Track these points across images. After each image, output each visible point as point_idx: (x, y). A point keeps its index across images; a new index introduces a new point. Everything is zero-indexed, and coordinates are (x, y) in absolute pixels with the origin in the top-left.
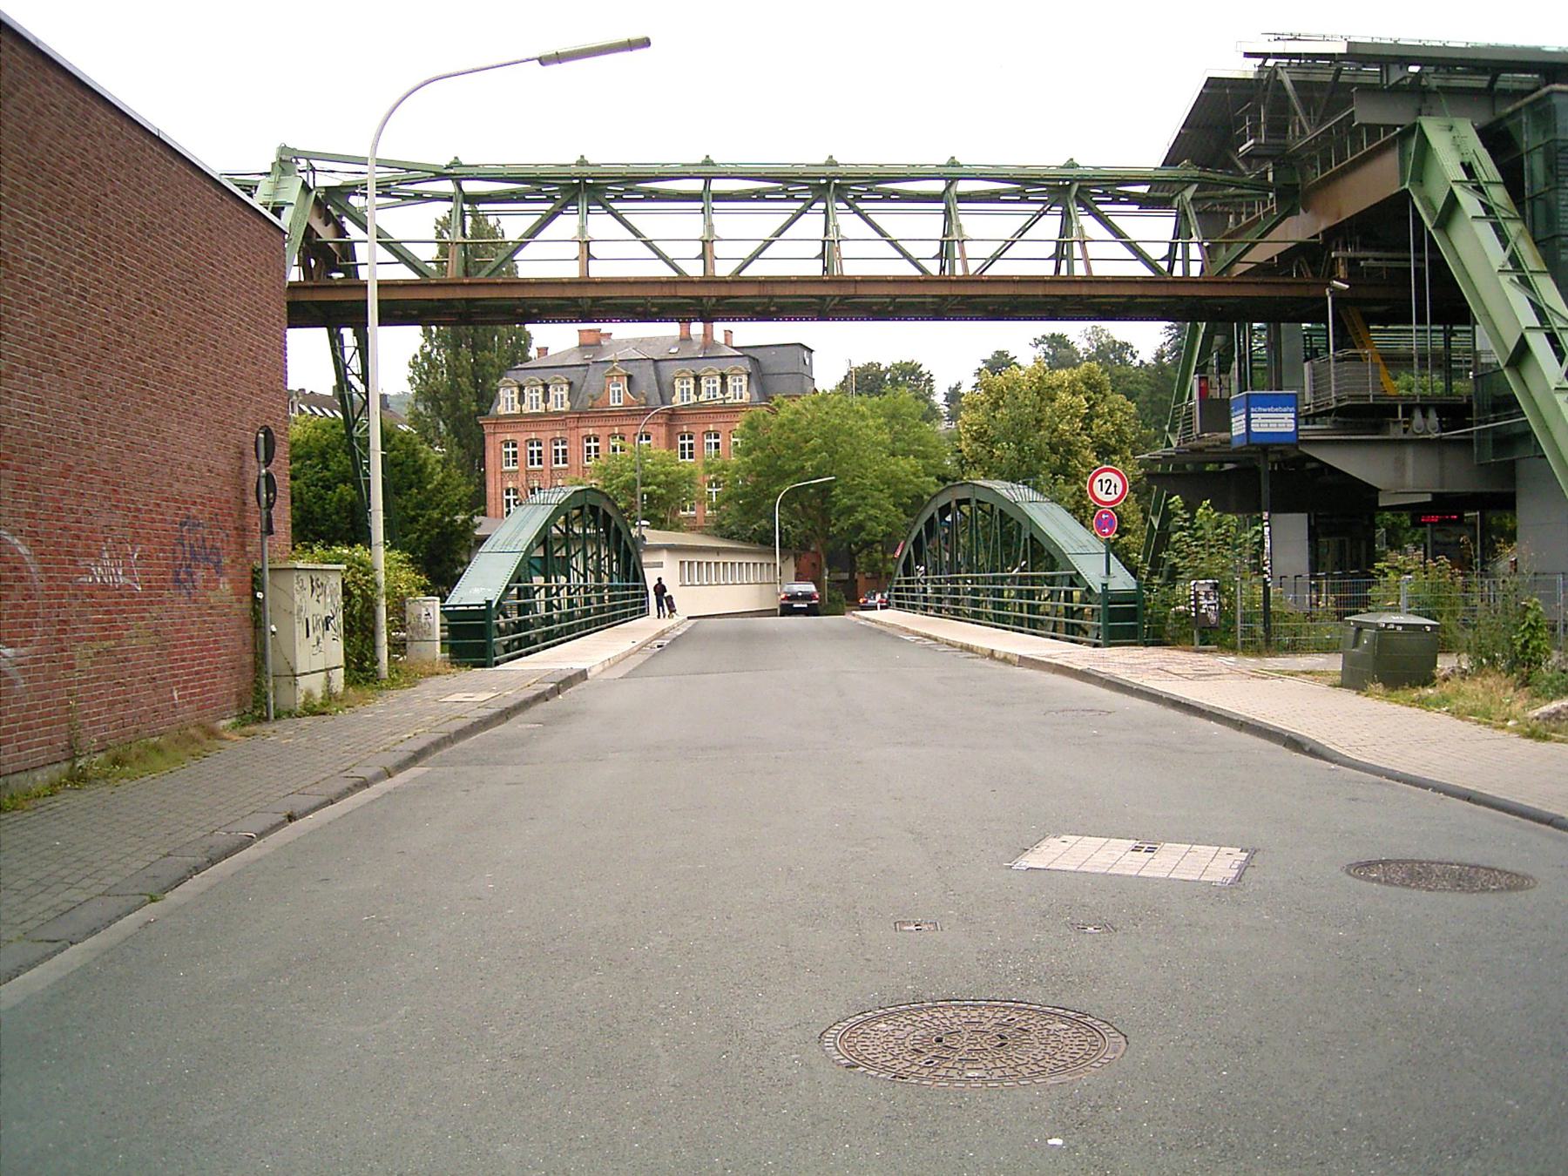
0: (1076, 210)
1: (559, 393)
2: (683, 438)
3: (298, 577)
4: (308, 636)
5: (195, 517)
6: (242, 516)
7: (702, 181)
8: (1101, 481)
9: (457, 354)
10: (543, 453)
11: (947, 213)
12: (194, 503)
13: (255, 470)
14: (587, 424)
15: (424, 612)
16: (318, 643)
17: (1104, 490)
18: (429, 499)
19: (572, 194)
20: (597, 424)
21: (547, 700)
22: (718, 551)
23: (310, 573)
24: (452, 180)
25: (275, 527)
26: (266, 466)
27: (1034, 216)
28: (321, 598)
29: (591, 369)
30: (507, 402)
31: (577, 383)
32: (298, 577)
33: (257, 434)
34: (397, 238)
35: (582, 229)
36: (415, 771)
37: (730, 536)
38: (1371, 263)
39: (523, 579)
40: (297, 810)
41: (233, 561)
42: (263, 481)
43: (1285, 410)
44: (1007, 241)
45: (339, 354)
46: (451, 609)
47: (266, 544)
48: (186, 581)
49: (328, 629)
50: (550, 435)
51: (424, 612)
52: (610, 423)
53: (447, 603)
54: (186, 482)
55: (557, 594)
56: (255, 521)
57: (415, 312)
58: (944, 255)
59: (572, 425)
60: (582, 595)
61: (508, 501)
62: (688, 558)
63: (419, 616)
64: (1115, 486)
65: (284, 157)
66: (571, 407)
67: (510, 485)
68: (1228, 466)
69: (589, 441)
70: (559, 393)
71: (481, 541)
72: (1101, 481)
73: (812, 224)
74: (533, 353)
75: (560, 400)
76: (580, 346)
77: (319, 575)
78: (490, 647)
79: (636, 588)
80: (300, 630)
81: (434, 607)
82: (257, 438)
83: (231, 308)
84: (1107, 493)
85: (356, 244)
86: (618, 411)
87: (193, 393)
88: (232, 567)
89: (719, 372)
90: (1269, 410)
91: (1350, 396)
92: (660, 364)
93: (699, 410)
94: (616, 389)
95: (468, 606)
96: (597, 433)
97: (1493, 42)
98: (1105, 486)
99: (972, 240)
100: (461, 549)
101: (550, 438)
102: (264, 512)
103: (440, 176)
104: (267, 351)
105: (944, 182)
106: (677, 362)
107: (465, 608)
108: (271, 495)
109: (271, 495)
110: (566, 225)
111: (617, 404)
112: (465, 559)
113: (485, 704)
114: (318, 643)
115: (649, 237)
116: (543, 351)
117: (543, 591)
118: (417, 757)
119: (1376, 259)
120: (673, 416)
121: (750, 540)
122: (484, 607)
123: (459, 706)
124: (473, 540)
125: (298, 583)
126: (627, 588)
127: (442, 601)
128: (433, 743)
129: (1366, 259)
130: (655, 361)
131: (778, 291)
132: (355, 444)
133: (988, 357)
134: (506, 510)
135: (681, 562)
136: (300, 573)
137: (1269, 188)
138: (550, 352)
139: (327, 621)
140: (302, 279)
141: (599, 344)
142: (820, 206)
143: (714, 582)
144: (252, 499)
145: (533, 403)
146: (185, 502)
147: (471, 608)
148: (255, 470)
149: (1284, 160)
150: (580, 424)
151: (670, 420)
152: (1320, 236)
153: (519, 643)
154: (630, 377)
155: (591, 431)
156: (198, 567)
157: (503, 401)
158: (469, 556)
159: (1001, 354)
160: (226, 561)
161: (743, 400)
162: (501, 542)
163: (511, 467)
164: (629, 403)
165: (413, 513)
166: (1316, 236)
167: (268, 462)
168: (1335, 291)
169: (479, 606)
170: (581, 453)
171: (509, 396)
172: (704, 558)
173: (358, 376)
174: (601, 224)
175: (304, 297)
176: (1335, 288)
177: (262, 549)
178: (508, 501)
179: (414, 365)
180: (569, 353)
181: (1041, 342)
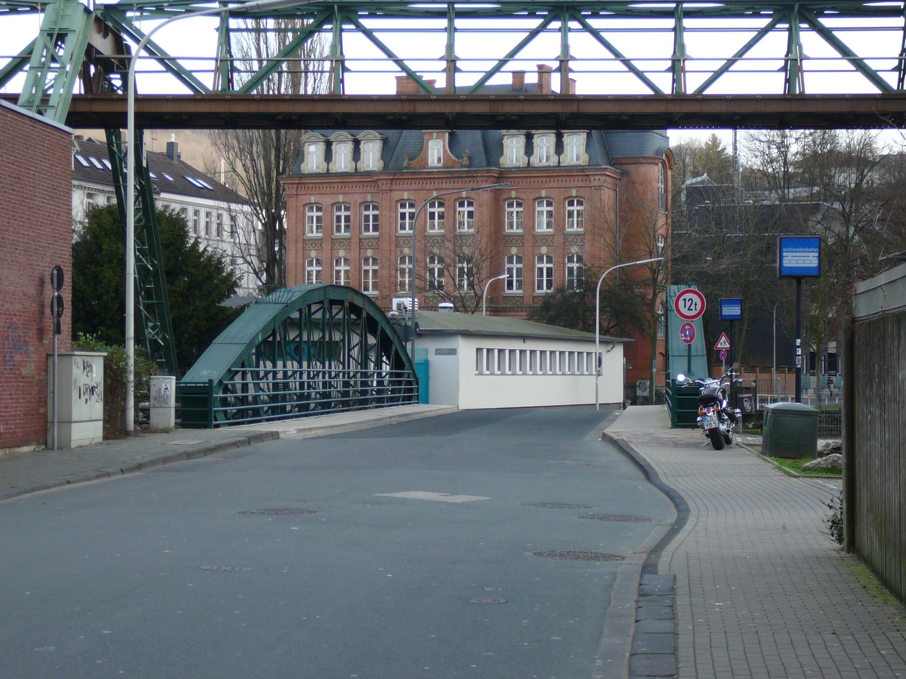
4: (80, 397)
5: (15, 323)
6: (41, 320)
8: (685, 300)
10: (351, 219)
11: (678, 31)
12: (15, 315)
13: (50, 293)
15: (163, 387)
17: (687, 306)
19: (328, 13)
20: (413, 187)
21: (238, 447)
22: (524, 338)
23: (83, 358)
25: (62, 328)
26: (58, 291)
28: (89, 374)
33: (53, 270)
36: (137, 473)
37: (551, 321)
39: (246, 364)
40: (71, 481)
41: (35, 350)
42: (55, 301)
43: (810, 250)
45: (115, 149)
46: (184, 385)
47: (56, 339)
48: (9, 361)
49: (93, 394)
50: (358, 198)
51: (163, 387)
53: (182, 381)
54: (11, 303)
55: (354, 376)
56: (49, 322)
58: (677, 67)
60: (298, 379)
62: (486, 344)
63: (160, 390)
64: (696, 304)
69: (403, 206)
72: (685, 300)
77: (89, 359)
80: (75, 394)
82: (52, 272)
83: (39, 193)
84: (689, 309)
87: (16, 249)
88: (35, 353)
90: (797, 250)
95: (196, 383)
96: (412, 197)
98: (688, 304)
99: (693, 59)
101: (359, 201)
102: (56, 319)
104: (59, 215)
107: (194, 385)
108: (60, 309)
109: (60, 309)
118: (139, 467)
122: (208, 385)
127: (177, 379)
128: (151, 461)
135: (479, 350)
139: (92, 390)
140: (83, 92)
142: (556, 25)
143: (567, 372)
144: (48, 311)
146: (10, 315)
148: (50, 293)
150: (393, 187)
155: (406, 195)
156: (16, 353)
160: (32, 349)
164: (450, 164)
167: (59, 287)
169: (205, 383)
170: (393, 220)
172: (507, 345)
175: (84, 108)
177: (54, 341)
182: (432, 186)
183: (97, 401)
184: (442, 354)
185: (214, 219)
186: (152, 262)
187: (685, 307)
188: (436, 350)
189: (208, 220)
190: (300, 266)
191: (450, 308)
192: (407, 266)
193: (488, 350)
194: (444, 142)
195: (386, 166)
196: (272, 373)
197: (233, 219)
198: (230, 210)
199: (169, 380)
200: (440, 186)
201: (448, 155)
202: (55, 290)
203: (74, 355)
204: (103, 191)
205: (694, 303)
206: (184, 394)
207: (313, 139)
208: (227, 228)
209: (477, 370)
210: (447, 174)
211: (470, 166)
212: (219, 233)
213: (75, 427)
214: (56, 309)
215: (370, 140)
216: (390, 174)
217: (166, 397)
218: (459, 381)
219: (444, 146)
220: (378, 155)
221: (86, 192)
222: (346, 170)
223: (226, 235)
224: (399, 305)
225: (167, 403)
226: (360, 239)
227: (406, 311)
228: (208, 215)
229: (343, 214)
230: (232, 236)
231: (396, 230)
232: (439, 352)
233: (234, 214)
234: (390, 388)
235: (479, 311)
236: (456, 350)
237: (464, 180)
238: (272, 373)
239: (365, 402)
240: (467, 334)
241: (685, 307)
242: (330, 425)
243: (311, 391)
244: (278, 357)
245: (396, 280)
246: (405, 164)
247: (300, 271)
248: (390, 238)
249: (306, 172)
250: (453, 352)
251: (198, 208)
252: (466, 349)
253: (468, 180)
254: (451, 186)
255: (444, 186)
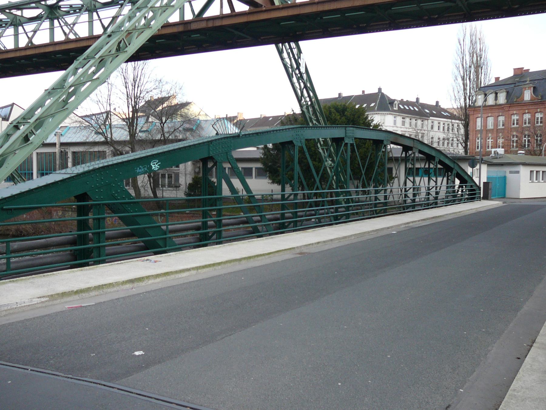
14: (513, 109)
52: (524, 108)
62: (535, 169)
85: (15, 105)
86: (528, 103)
97: (381, 1)
101: (497, 115)
135: (531, 171)
150: (510, 109)
153: (384, 211)
164: (533, 99)
170: (510, 122)
184: (512, 173)
185: (446, 125)
188: (510, 171)
189: (439, 125)
190: (474, 141)
191: (523, 153)
192: (515, 139)
193: (537, 172)
194: (531, 91)
195: (507, 102)
196: (293, 195)
197: (453, 125)
198: (452, 122)
200: (529, 108)
201: (533, 96)
204: (408, 117)
207: (480, 93)
208: (451, 128)
209: (530, 180)
210: (532, 103)
211: (542, 99)
212: (448, 130)
215: (502, 92)
216: (508, 104)
218: (520, 185)
219: (531, 93)
220: (505, 98)
221: (402, 117)
222: (492, 104)
223: (451, 131)
224: (495, 152)
226: (497, 130)
227: (498, 154)
228: (444, 124)
230: (452, 131)
231: (511, 126)
232: (511, 172)
233: (453, 123)
234: (467, 193)
235: (541, 156)
236: (519, 171)
237: (539, 105)
238: (293, 195)
239: (454, 201)
240: (524, 164)
242: (375, 229)
243: (406, 199)
244: (416, 175)
245: (510, 144)
246: (515, 100)
247: (474, 142)
248: (508, 128)
249: (477, 106)
250: (518, 172)
251: (433, 121)
252: (525, 172)
253: (540, 105)
254: (533, 107)
255: (530, 108)
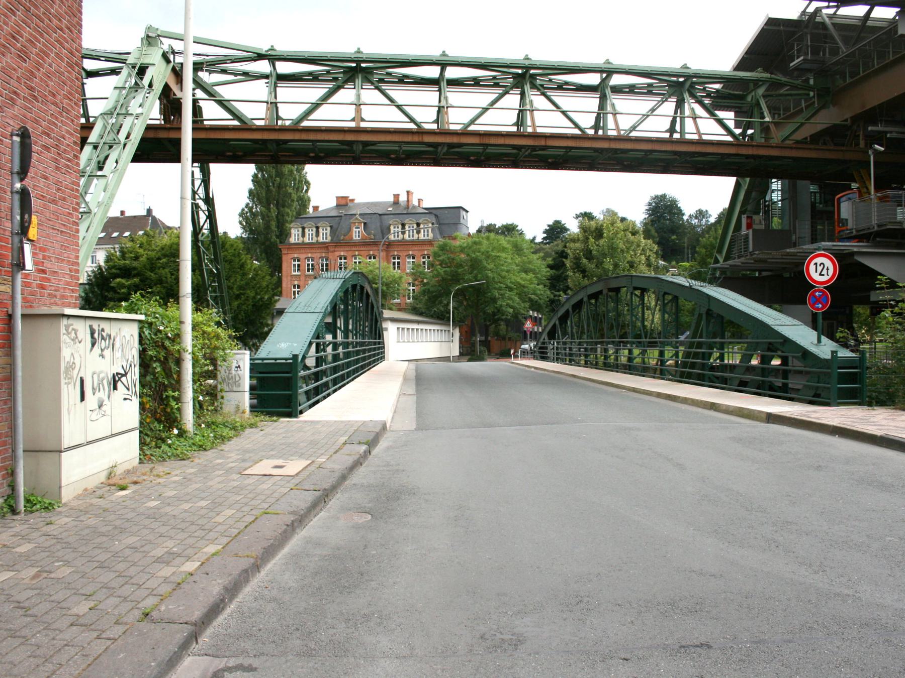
0: (686, 96)
1: (325, 232)
2: (394, 258)
3: (67, 327)
4: (83, 398)
7: (438, 69)
9: (269, 209)
15: (234, 364)
16: (100, 406)
17: (819, 271)
18: (247, 284)
22: (418, 322)
23: (89, 322)
24: (269, 60)
26: (22, 180)
27: (659, 101)
29: (343, 218)
30: (295, 236)
31: (335, 226)
32: (67, 327)
34: (227, 98)
35: (358, 96)
37: (421, 314)
38: (894, 135)
44: (644, 115)
49: (115, 388)
50: (319, 255)
53: (256, 356)
57: (240, 154)
59: (332, 250)
61: (294, 292)
64: (828, 269)
65: (150, 34)
66: (332, 240)
67: (296, 283)
68: (764, 274)
70: (325, 232)
71: (281, 312)
72: (816, 264)
73: (512, 100)
74: (311, 210)
75: (325, 235)
76: (337, 206)
77: (105, 325)
78: (296, 398)
79: (379, 343)
81: (243, 360)
84: (820, 274)
89: (415, 221)
91: (890, 222)
92: (383, 217)
93: (403, 243)
94: (357, 230)
95: (276, 359)
98: (820, 269)
100: (268, 315)
103: (260, 57)
105: (598, 75)
106: (392, 216)
107: (273, 361)
109: (26, 216)
110: (346, 94)
111: (357, 238)
112: (270, 322)
113: (297, 482)
114: (100, 406)
115: (400, 103)
116: (316, 208)
117: (331, 346)
119: (897, 132)
120: (390, 245)
121: (432, 317)
122: (291, 361)
123: (267, 484)
124: (275, 311)
125: (68, 333)
126: (362, 344)
129: (891, 132)
130: (380, 215)
131: (493, 141)
132: (200, 245)
133: (551, 223)
134: (293, 297)
136: (71, 321)
137: (811, 88)
138: (320, 209)
141: (346, 205)
145: (310, 237)
147: (278, 361)
149: (823, 72)
151: (387, 248)
152: (849, 120)
154: (365, 224)
155: (342, 254)
157: (293, 236)
158: (272, 320)
159: (557, 222)
161: (429, 238)
162: (303, 304)
163: (297, 273)
165: (238, 292)
166: (846, 120)
167: (23, 173)
168: (876, 152)
169: (286, 359)
171: (297, 233)
173: (203, 200)
174: (370, 95)
176: (876, 150)
178: (294, 292)
179: (242, 214)
180: (332, 209)
181: (579, 217)
182: (356, 249)
183: (125, 399)
186: (216, 266)
187: (816, 272)
199: (242, 356)
202: (16, 177)
203: (64, 315)
205: (826, 268)
206: (260, 373)
213: (67, 458)
214: (18, 218)
217: (237, 379)
225: (239, 385)
229: (311, 263)
241: (816, 272)
246: (342, 238)
